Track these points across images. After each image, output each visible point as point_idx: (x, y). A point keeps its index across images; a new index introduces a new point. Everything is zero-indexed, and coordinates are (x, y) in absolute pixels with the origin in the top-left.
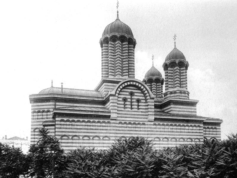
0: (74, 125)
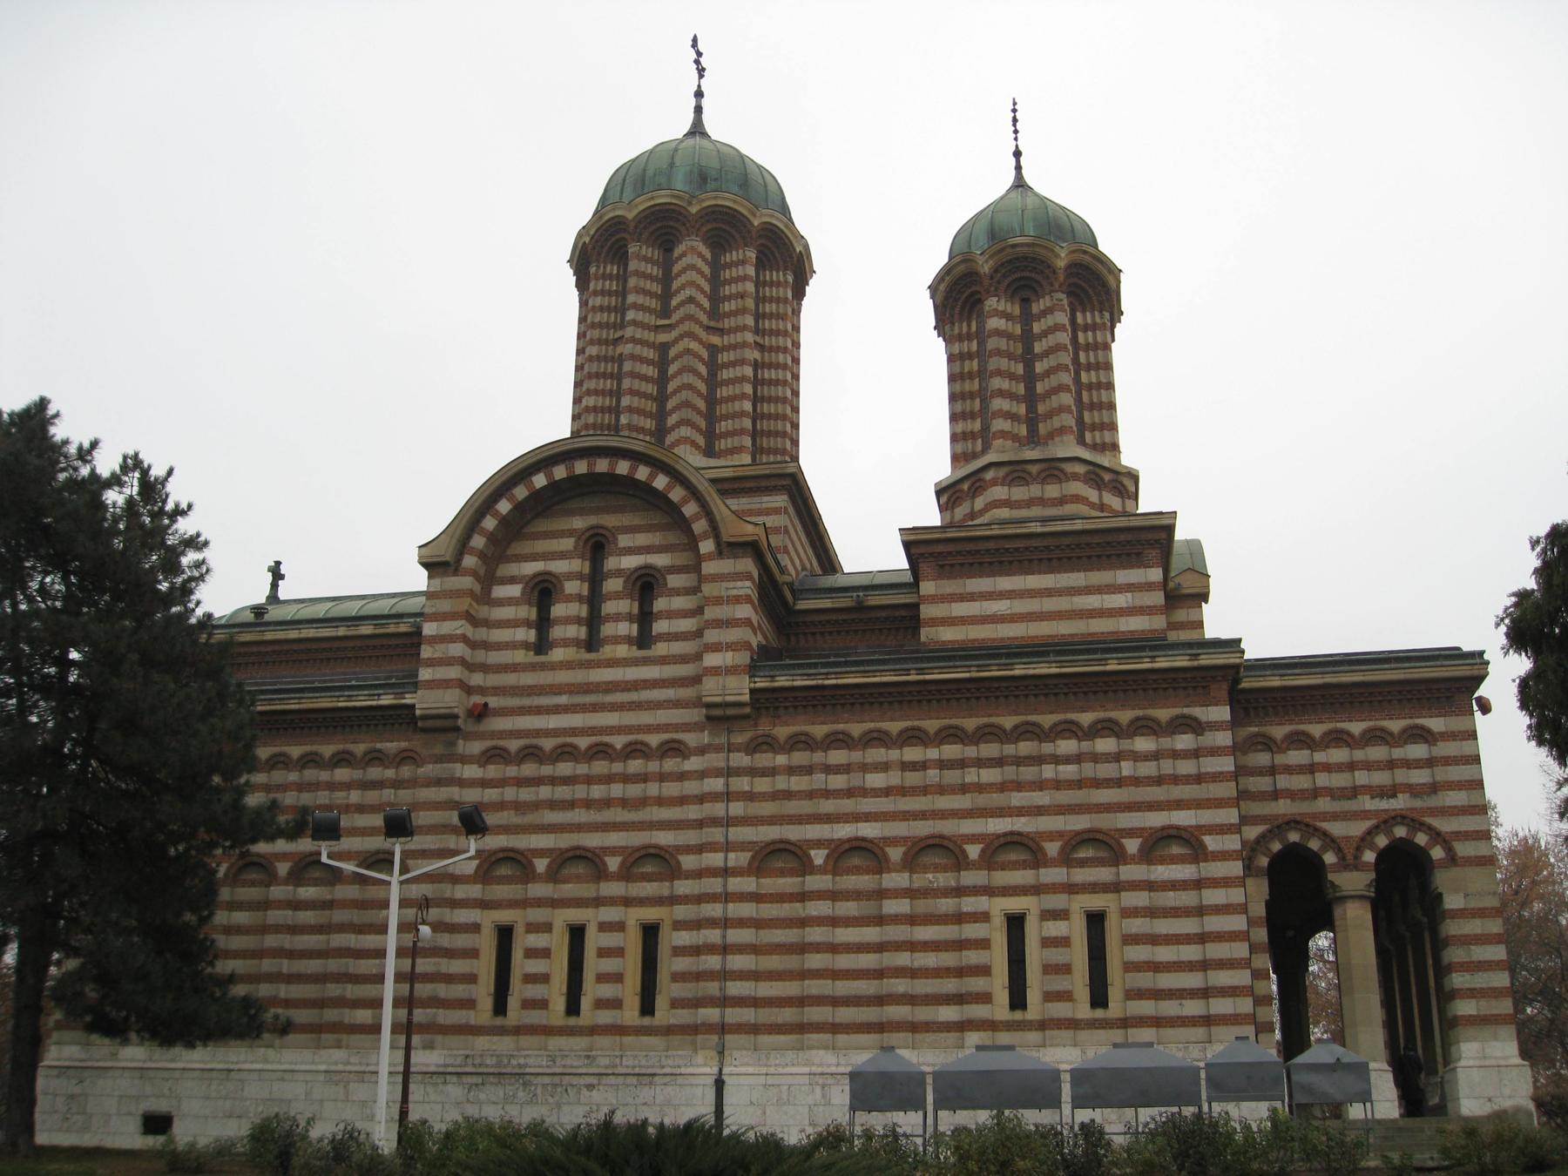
0: (682, 776)
